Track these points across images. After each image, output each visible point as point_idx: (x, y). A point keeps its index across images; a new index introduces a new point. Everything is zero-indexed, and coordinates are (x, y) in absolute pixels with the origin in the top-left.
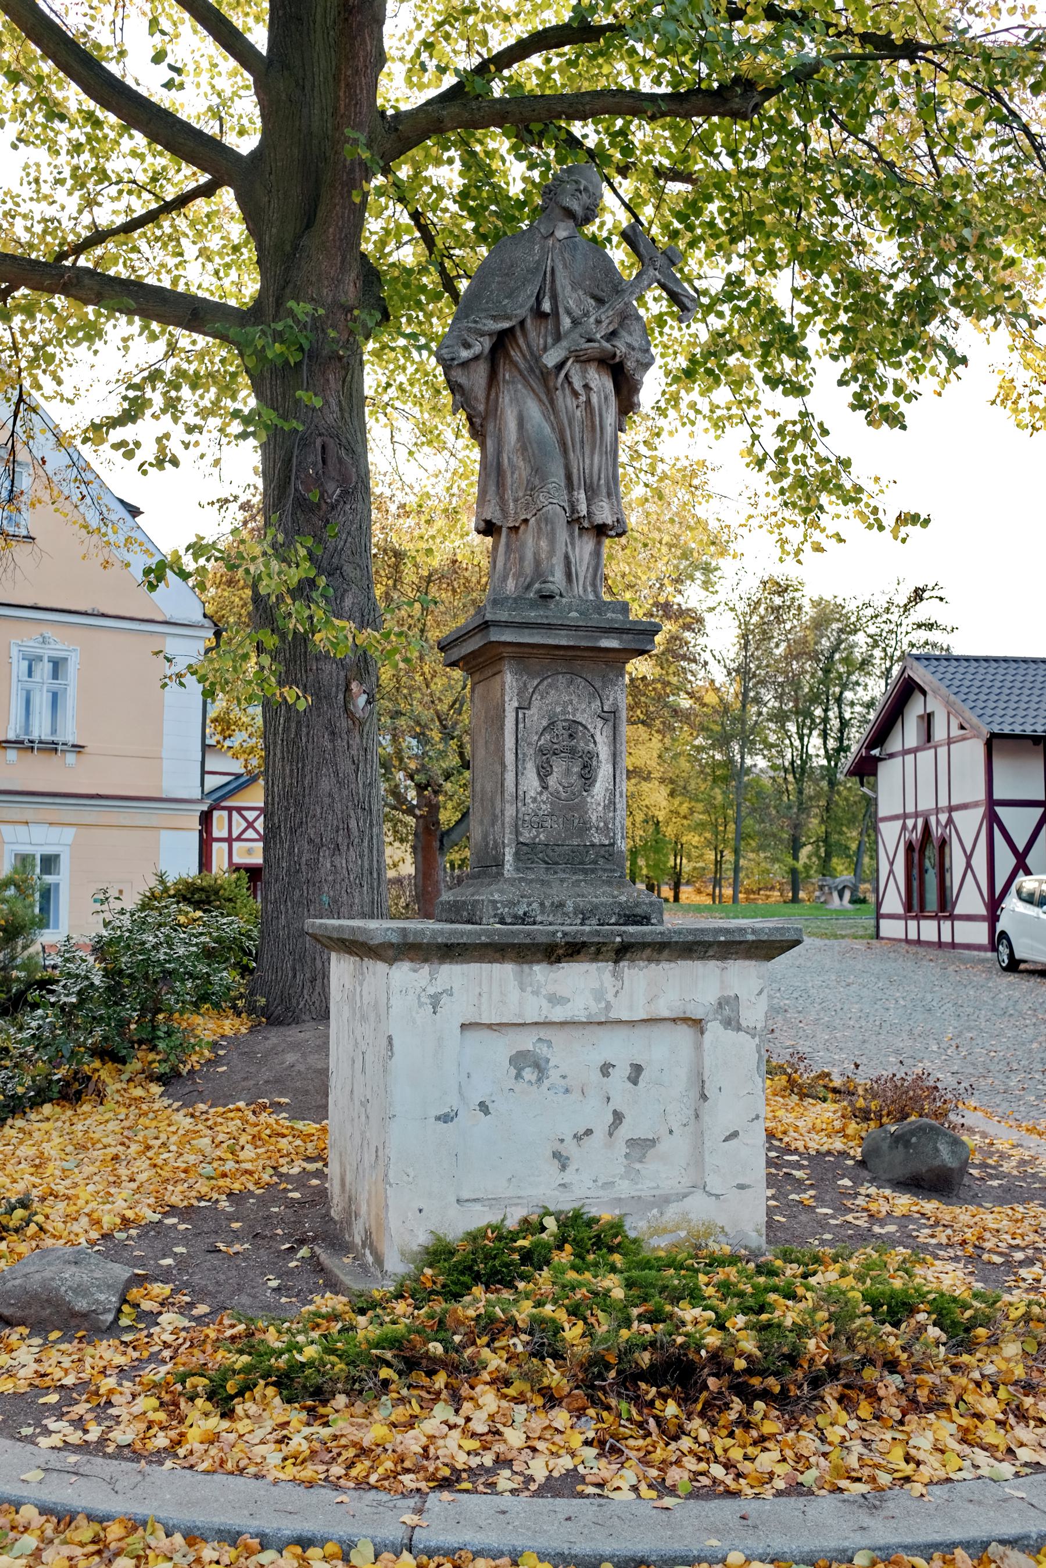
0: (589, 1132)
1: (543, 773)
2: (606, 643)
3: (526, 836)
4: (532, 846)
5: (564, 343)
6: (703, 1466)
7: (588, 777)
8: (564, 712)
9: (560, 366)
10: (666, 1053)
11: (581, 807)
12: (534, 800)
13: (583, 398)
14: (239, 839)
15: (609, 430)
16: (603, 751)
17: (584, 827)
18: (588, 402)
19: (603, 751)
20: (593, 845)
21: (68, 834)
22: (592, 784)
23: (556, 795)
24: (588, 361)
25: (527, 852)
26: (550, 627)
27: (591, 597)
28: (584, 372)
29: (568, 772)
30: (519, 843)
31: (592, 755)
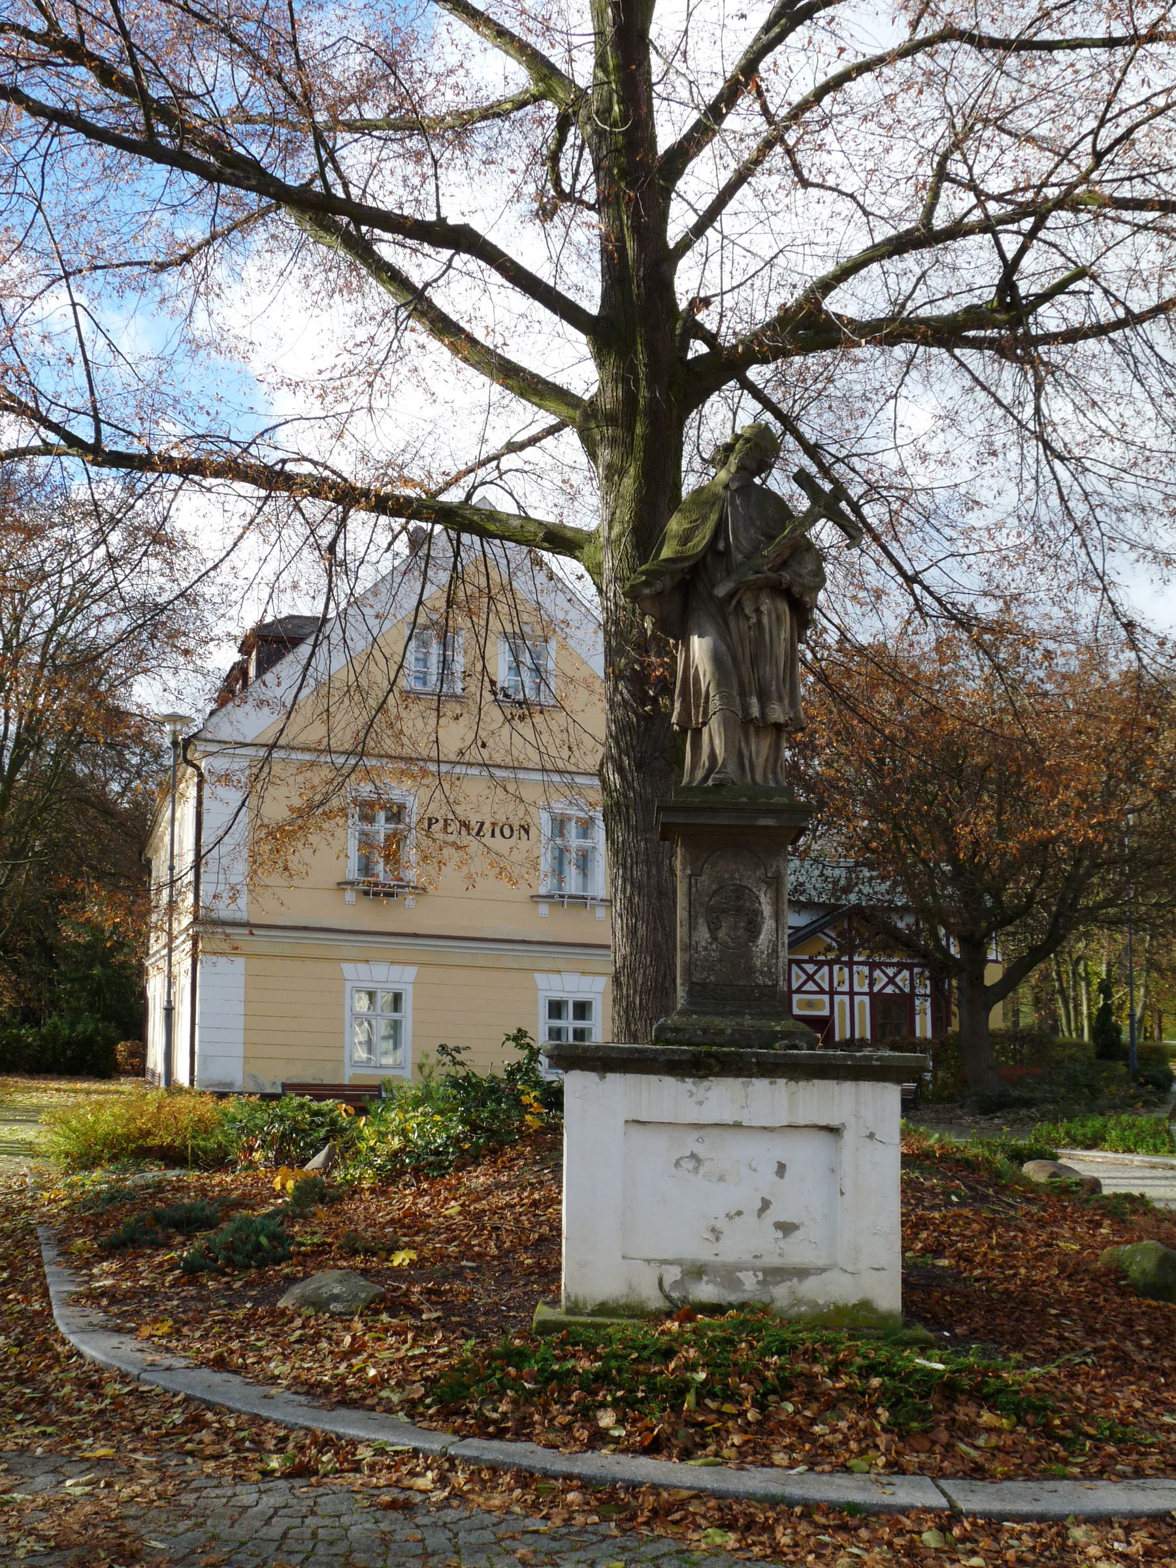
0: (739, 1213)
1: (713, 929)
2: (762, 822)
3: (698, 977)
4: (704, 985)
5: (735, 577)
6: (502, 1530)
7: (753, 929)
8: (732, 878)
9: (731, 595)
10: (806, 1154)
11: (749, 956)
12: (705, 949)
13: (754, 620)
14: (799, 991)
15: (781, 649)
16: (767, 910)
17: (750, 970)
18: (760, 622)
19: (767, 910)
20: (758, 986)
21: (411, 972)
22: (757, 936)
23: (725, 945)
24: (760, 589)
25: (697, 991)
26: (714, 810)
27: (772, 784)
28: (757, 599)
29: (735, 927)
30: (692, 983)
31: (758, 913)
